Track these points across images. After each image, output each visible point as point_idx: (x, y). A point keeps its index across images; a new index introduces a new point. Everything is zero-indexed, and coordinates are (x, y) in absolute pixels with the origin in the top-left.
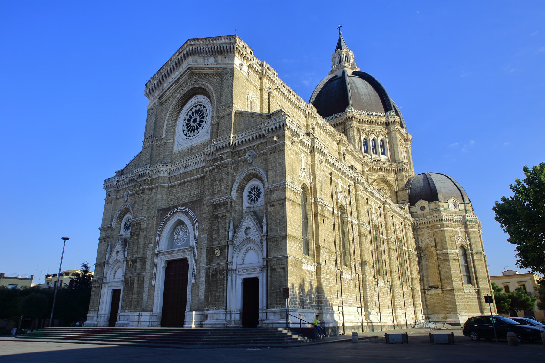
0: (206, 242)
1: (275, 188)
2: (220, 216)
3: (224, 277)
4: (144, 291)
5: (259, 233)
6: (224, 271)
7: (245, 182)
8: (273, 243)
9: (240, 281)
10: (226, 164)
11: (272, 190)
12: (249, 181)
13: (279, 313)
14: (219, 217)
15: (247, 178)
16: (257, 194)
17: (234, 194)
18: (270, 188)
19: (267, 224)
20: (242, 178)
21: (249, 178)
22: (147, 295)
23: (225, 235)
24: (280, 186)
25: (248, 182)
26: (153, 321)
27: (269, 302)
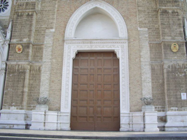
0: (147, 36)
2: (170, 11)
4: (41, 84)
5: (2, 38)
14: (168, 13)
19: (12, 31)
22: (48, 90)
23: (180, 31)
26: (61, 122)
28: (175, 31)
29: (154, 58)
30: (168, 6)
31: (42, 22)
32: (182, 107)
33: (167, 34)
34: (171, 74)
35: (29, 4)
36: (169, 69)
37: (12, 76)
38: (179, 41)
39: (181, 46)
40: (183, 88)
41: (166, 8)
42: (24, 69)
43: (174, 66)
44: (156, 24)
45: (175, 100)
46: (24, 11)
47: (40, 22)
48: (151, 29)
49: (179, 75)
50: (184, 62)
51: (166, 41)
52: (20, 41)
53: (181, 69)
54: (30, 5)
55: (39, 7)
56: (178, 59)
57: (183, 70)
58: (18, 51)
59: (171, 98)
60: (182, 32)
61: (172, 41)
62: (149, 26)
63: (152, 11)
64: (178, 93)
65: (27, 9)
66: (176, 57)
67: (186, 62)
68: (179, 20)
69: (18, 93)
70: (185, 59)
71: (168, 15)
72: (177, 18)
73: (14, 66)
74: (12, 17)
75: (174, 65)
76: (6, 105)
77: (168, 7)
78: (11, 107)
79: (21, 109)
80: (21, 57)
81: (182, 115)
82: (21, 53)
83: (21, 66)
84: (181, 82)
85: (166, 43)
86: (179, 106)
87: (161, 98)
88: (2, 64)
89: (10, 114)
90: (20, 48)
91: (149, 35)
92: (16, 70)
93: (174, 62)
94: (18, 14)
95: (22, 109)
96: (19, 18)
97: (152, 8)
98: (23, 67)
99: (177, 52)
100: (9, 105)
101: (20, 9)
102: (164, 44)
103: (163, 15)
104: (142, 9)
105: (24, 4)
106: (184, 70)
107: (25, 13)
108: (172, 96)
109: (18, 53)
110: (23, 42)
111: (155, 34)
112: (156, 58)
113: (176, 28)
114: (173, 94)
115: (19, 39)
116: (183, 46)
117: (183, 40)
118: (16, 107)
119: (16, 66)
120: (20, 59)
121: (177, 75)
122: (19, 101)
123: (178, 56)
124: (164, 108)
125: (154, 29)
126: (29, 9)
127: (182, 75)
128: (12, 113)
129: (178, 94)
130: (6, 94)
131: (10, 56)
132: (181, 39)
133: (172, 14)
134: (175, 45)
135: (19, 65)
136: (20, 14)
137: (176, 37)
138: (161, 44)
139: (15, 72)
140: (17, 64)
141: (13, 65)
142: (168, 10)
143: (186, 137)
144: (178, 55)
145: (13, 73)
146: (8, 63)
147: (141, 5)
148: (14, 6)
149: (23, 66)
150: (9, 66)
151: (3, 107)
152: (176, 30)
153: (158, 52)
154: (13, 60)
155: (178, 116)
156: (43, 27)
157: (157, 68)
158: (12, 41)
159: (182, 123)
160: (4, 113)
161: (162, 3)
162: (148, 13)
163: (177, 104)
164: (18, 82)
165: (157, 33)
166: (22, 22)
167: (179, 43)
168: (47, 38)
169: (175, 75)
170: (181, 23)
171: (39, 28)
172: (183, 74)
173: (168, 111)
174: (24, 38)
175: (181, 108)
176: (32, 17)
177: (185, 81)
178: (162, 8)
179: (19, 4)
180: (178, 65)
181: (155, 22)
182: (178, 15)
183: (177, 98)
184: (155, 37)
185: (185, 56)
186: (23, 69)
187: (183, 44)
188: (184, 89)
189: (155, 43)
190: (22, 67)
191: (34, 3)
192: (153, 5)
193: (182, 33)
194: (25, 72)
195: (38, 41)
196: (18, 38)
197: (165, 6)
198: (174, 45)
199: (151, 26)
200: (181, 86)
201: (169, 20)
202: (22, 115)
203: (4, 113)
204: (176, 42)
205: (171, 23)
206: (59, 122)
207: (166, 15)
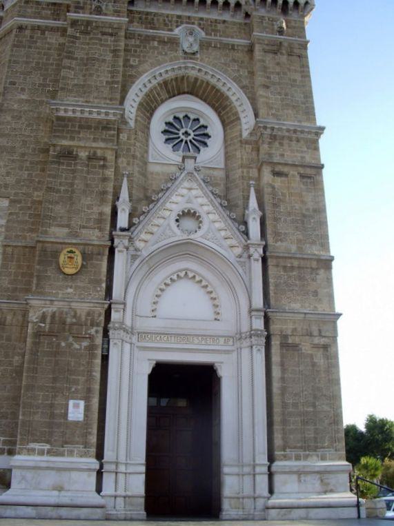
1: (287, 134)
2: (83, 154)
3: (92, 348)
6: (92, 325)
7: (164, 95)
8: (285, 271)
9: (144, 370)
10: (112, 28)
11: (275, 136)
12: (174, 96)
13: (318, 476)
14: (76, 157)
15: (173, 87)
16: (195, 135)
17: (131, 107)
18: (273, 129)
20: (159, 79)
21: (174, 88)
23: (101, 214)
24: (302, 132)
25: (170, 97)
27: (278, 441)
28: (85, 211)
29: (8, 288)
30: (80, 139)
32: (66, 443)
33: (59, 219)
34: (46, 341)
36: (43, 325)
38: (89, 242)
39: (95, 256)
40: (78, 384)
41: (71, 143)
43: (61, 317)
44: (37, 191)
45: (48, 420)
48: (19, 202)
49: (70, 345)
50: (92, 305)
51: (48, 240)
53: (82, 325)
56: (76, 297)
57: (86, 330)
59: (34, 413)
60: (104, 217)
61: (66, 241)
62: (16, 194)
63: (34, 150)
64: (59, 400)
66: (70, 290)
67: (97, 305)
68: (105, 179)
70: (97, 299)
71: (75, 164)
72: (99, 174)
75: (61, 313)
77: (80, 140)
81: (59, 470)
84: (74, 367)
85: (50, 245)
86: (55, 441)
87: (9, 411)
88: (253, 318)
91: (8, 221)
93: (61, 303)
97: (38, 142)
99: (77, 273)
102: (42, 248)
103: (59, 163)
104: (5, 144)
106: (89, 332)
108: (39, 408)
111: (27, 218)
112: (15, 290)
113: (90, 203)
114: (42, 403)
116: (99, 257)
117: (103, 239)
121: (63, 344)
123: (76, 288)
124: (14, 443)
125: (29, 203)
127: (81, 345)
129: (58, 404)
132: (97, 237)
133: (87, 162)
134: (71, 252)
137: (84, 231)
138: (34, 248)
142: (77, 151)
144: (79, 284)
147: (7, 132)
152: (88, 208)
153: (25, 271)
155: (48, 472)
157: (12, 320)
159: (56, 493)
161: (65, 129)
162: (23, 155)
163: (51, 434)
165: (36, 215)
167: (90, 247)
168: (167, 400)
169: (59, 345)
170: (108, 189)
172: (85, 343)
173: (19, 454)
175: (63, 447)
177: (88, 363)
178: (60, 143)
180: (72, 313)
181: (36, 184)
182: (104, 167)
183: (52, 415)
184: (26, 227)
185: (99, 289)
187: (101, 251)
188: (79, 387)
189: (20, 244)
192: (43, 134)
193: (105, 220)
197: (72, 139)
198: (68, 252)
199: (20, 195)
200: (74, 379)
201: (75, 178)
204: (79, 244)
205: (79, 188)
207: (67, 165)
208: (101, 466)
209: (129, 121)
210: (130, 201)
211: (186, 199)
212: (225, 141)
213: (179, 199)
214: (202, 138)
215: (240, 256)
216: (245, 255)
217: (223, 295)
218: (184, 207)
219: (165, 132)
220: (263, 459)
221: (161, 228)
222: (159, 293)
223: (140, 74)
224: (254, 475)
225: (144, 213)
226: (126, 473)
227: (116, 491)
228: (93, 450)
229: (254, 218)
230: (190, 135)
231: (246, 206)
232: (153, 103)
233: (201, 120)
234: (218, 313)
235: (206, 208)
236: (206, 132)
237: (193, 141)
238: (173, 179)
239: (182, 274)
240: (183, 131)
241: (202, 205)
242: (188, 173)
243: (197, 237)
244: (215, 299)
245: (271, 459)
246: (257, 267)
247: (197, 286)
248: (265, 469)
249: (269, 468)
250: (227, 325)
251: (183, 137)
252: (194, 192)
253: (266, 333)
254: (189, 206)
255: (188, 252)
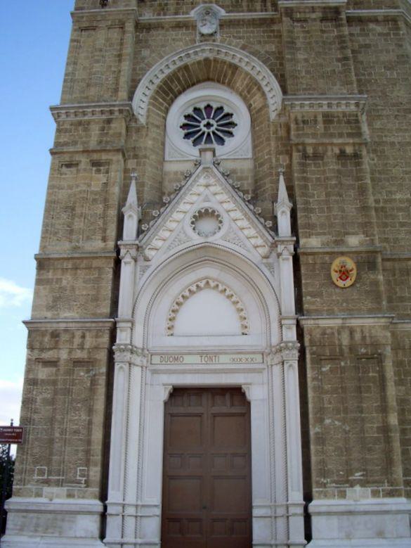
31: (388, 181)
35: (335, 119)
37: (331, 370)
42: (375, 345)
46: (326, 141)
47: (380, 180)
52: (337, 243)
54: (339, 122)
55: (365, 132)
58: (340, 278)
65: (332, 135)
69: (367, 435)
73: (333, 333)
74: (274, 160)
76: (325, 481)
78: (347, 489)
79: (391, 494)
80: (353, 300)
82: (352, 285)
83: (362, 332)
89: (351, 518)
90: (347, 267)
92: (344, 347)
94: (304, 150)
95: (393, 496)
96: (309, 164)
98: (368, 339)
100: (336, 482)
101: (307, 135)
105: (315, 117)
107: (329, 148)
109: (337, 287)
110: (348, 247)
115: (330, 237)
118: (369, 489)
119: (343, 333)
120: (353, 310)
122: (378, 466)
126: (341, 135)
128: (362, 510)
130: (321, 440)
131: (309, 298)
135: (352, 331)
136: (310, 150)
139: (341, 357)
140: (343, 327)
141: (328, 331)
143: (409, 511)
145: (332, 359)
146: (309, 322)
148: (271, 124)
149: (370, 334)
150: (314, 334)
151: (314, 490)
154: (324, 310)
156: (398, 197)
158: (305, 243)
160: (328, 514)
164: (361, 393)
166: (327, 178)
171: (386, 201)
174: (348, 234)
176: (358, 164)
179: (300, 118)
186: (372, 344)
190: (364, 338)
191: (353, 115)
194: (380, 354)
195: (392, 244)
196: (324, 234)
202: (399, 516)
203: (328, 514)
206: (139, 503)
208: (105, 508)
209: (140, 117)
210: (139, 205)
211: (202, 198)
212: (253, 126)
213: (195, 198)
214: (227, 124)
215: (267, 257)
216: (274, 254)
217: (249, 301)
218: (201, 206)
219: (184, 126)
220: (297, 496)
221: (174, 234)
222: (176, 307)
223: (149, 66)
224: (288, 517)
225: (155, 217)
226: (136, 517)
227: (122, 537)
228: (96, 490)
229: (283, 212)
230: (212, 125)
231: (274, 199)
232: (168, 95)
233: (212, 104)
234: (246, 327)
235: (226, 206)
236: (230, 120)
237: (216, 132)
238: (187, 176)
239: (202, 284)
240: (204, 122)
241: (222, 203)
242: (204, 168)
243: (217, 239)
244: (242, 310)
245: (308, 497)
246: (287, 268)
247: (222, 297)
248: (300, 510)
249: (306, 508)
250: (255, 340)
251: (204, 129)
252: (212, 189)
253: (299, 345)
254: (206, 205)
255: (207, 258)
